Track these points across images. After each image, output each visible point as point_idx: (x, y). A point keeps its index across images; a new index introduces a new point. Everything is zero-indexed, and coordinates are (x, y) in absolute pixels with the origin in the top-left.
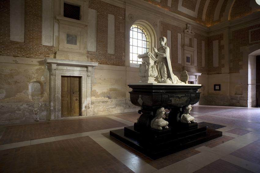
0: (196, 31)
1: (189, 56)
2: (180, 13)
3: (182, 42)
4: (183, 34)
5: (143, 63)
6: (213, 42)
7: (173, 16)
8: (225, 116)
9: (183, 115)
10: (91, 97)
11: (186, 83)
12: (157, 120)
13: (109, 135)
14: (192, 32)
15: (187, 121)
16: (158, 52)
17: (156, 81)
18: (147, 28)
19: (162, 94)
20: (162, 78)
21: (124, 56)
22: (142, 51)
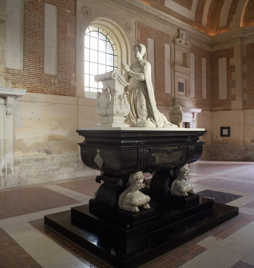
0: (192, 41)
1: (182, 81)
2: (169, 11)
3: (171, 58)
4: (173, 45)
5: (105, 90)
6: (219, 59)
7: (156, 14)
8: (239, 178)
9: (175, 181)
10: (14, 152)
11: (179, 126)
12: (130, 195)
13: (44, 223)
14: (188, 43)
15: (183, 193)
16: (131, 71)
17: (127, 123)
18: (113, 32)
19: (138, 147)
20: (138, 117)
21: (74, 79)
22: (103, 71)
